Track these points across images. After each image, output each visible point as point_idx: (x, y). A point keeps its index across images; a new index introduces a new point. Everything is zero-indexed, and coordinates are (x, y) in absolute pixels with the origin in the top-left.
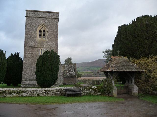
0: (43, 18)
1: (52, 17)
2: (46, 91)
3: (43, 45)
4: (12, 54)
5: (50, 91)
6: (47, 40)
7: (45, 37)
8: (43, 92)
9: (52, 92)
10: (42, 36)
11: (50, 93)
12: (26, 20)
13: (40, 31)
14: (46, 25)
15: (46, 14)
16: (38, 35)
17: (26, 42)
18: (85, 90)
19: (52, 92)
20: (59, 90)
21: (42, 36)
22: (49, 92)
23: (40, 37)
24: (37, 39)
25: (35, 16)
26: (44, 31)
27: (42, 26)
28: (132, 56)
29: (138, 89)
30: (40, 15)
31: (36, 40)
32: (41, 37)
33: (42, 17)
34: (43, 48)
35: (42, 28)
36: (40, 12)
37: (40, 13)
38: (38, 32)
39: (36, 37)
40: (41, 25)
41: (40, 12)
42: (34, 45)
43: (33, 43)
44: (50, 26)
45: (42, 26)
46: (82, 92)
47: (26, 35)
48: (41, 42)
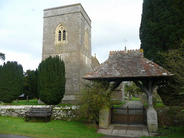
0: (61, 15)
1: (73, 12)
2: (9, 110)
3: (62, 50)
4: (50, 57)
5: (13, 110)
6: (67, 42)
7: (65, 39)
8: (5, 111)
9: (16, 113)
10: (62, 38)
11: (13, 113)
12: (45, 22)
13: (60, 32)
14: (66, 23)
15: (65, 9)
16: (57, 38)
17: (44, 47)
18: (59, 112)
19: (16, 113)
20: (24, 109)
21: (62, 38)
22: (13, 112)
23: (60, 40)
24: (55, 43)
25: (53, 15)
26: (64, 31)
27: (61, 25)
28: (123, 69)
29: (156, 115)
30: (59, 12)
31: (55, 45)
32: (61, 40)
33: (61, 14)
34: (62, 53)
35: (62, 27)
36: (59, 8)
37: (59, 9)
38: (57, 33)
39: (54, 40)
40: (60, 24)
41: (59, 8)
42: (53, 51)
43: (52, 49)
44: (70, 24)
45: (61, 25)
46: (56, 114)
47: (44, 40)
48: (60, 46)
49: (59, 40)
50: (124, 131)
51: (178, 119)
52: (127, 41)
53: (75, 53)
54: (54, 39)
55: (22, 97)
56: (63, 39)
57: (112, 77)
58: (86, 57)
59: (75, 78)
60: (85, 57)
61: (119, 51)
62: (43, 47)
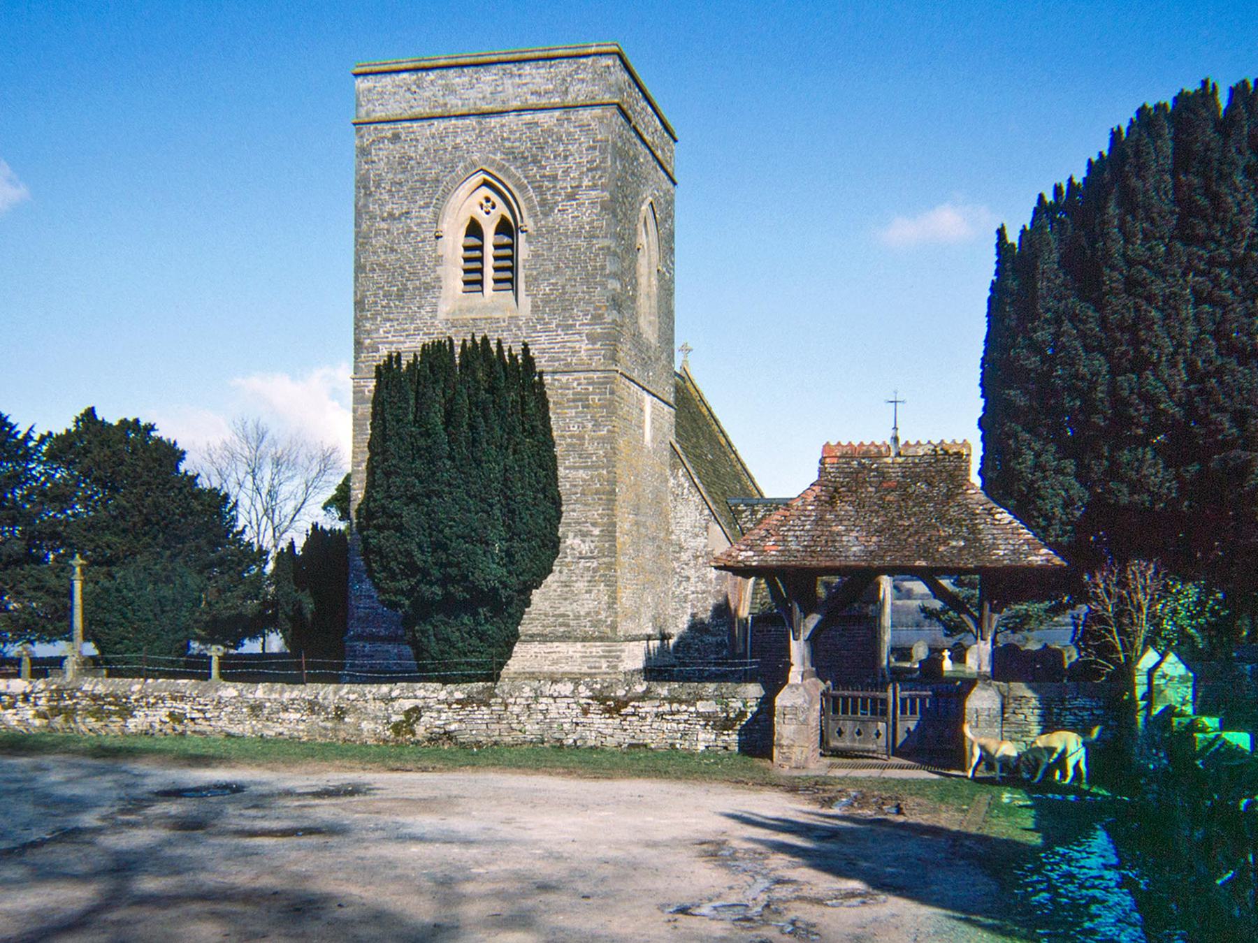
13: (474, 229)
16: (454, 276)
23: (474, 282)
26: (504, 228)
35: (488, 200)
38: (454, 241)
39: (432, 287)
49: (466, 283)
50: (879, 771)
51: (532, 427)
52: (896, 393)
53: (582, 375)
54: (438, 279)
55: (264, 656)
56: (496, 281)
57: (48, 890)
58: (648, 399)
59: (584, 535)
60: (640, 401)
61: (844, 443)
62: (356, 317)
